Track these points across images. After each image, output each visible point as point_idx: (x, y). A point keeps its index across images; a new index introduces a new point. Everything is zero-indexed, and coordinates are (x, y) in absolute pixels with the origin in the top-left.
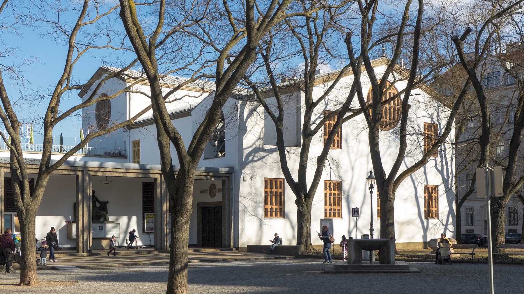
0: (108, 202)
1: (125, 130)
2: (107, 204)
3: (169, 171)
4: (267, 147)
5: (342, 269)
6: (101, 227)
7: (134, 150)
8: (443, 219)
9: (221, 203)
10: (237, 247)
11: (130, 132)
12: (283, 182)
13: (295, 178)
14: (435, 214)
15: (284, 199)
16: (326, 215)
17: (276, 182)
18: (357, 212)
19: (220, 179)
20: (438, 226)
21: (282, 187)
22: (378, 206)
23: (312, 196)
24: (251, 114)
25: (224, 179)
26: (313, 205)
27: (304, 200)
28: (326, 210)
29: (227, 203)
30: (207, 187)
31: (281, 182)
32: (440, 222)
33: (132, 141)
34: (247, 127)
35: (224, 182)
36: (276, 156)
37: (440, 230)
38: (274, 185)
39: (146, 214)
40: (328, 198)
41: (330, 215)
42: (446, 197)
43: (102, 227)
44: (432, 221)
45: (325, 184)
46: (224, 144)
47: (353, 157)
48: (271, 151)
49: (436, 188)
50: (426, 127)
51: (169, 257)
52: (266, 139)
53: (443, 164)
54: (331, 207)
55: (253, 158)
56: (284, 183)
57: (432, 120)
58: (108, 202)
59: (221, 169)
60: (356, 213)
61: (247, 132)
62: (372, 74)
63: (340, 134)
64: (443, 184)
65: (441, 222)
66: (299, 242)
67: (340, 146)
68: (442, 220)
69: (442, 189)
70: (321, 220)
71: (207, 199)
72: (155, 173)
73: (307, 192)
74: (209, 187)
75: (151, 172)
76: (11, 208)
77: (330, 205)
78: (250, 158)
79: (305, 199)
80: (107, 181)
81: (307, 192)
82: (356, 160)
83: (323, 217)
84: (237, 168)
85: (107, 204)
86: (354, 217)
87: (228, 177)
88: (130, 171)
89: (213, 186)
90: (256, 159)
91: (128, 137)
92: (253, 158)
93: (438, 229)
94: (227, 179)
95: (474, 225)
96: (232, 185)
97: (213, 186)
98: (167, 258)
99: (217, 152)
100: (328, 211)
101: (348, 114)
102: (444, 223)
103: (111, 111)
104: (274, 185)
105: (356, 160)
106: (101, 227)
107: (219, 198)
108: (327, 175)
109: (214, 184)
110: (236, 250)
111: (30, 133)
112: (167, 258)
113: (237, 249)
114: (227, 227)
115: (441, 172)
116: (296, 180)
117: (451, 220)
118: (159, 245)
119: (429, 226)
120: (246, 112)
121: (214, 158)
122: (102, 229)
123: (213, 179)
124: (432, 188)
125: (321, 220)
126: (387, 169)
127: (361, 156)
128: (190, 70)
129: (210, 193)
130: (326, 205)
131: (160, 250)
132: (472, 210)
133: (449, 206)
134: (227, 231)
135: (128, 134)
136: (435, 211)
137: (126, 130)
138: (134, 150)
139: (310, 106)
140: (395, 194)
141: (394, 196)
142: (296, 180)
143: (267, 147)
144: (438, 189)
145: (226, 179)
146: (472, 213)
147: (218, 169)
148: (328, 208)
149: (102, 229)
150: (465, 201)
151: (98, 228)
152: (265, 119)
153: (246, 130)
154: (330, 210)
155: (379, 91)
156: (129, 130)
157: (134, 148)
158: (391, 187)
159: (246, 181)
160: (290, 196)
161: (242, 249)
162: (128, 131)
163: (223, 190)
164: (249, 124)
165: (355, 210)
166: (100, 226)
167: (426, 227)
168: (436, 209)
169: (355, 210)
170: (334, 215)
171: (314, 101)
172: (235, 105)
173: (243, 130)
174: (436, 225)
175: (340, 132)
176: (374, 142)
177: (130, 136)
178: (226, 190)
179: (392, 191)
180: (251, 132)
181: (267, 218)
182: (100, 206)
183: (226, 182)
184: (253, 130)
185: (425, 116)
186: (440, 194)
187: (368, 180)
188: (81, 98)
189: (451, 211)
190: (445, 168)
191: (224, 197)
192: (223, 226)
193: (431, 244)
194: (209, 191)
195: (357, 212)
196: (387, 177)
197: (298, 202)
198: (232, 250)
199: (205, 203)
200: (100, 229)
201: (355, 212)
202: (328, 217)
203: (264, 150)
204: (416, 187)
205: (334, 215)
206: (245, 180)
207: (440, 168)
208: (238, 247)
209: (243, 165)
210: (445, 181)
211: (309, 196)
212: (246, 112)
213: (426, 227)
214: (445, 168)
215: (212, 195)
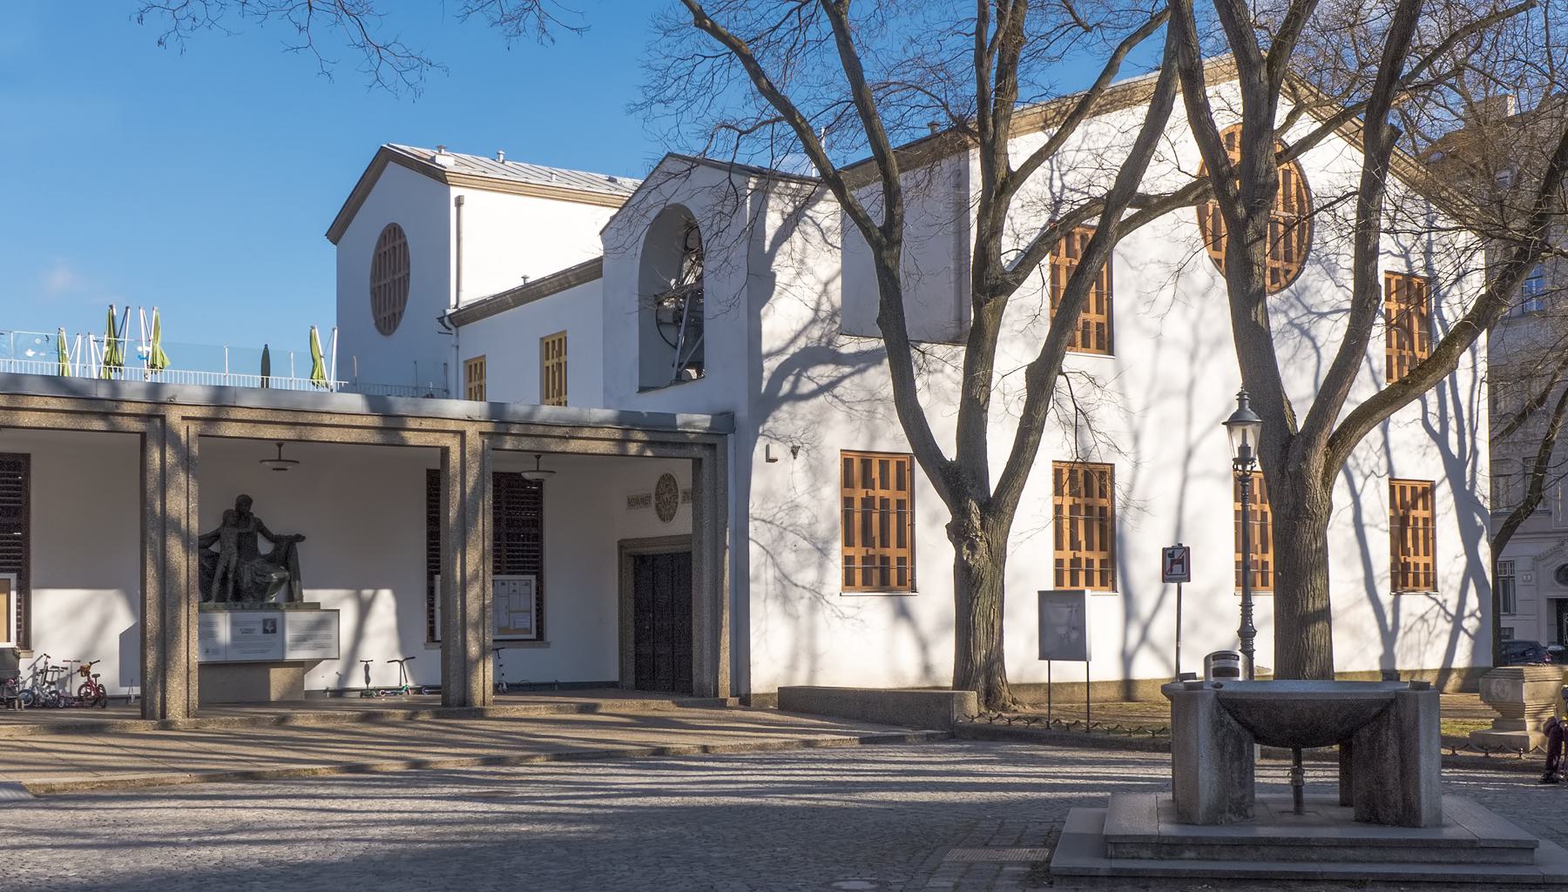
0: (299, 538)
1: (443, 329)
2: (298, 545)
4: (848, 345)
5: (1146, 853)
6: (269, 623)
7: (471, 389)
8: (1446, 597)
9: (686, 539)
10: (743, 692)
11: (457, 335)
12: (907, 467)
13: (949, 450)
14: (1427, 575)
15: (912, 525)
16: (1059, 579)
18: (1180, 562)
19: (682, 452)
20: (1432, 622)
21: (905, 482)
22: (1237, 551)
23: (1007, 510)
24: (791, 223)
25: (697, 452)
26: (1016, 544)
27: (977, 523)
28: (1059, 563)
29: (706, 537)
30: (650, 488)
31: (900, 465)
32: (1438, 607)
33: (466, 362)
34: (774, 275)
35: (698, 463)
36: (880, 378)
37: (1438, 636)
40: (1066, 524)
41: (1074, 582)
42: (1456, 524)
43: (274, 622)
44: (1414, 604)
45: (1058, 474)
46: (703, 341)
47: (1137, 400)
48: (864, 360)
49: (1426, 492)
50: (1393, 288)
52: (846, 319)
53: (1446, 413)
54: (1078, 554)
55: (795, 385)
56: (912, 470)
57: (1409, 264)
58: (299, 538)
59: (681, 419)
60: (1177, 568)
61: (777, 288)
62: (1237, 18)
63: (1105, 302)
64: (1447, 481)
65: (1441, 605)
66: (964, 677)
67: (1105, 343)
68: (1445, 601)
69: (1445, 499)
70: (1043, 596)
72: (441, 428)
73: (992, 494)
74: (655, 486)
75: (412, 424)
76: (8, 558)
77: (1075, 545)
78: (786, 387)
79: (982, 519)
80: (280, 460)
81: (992, 494)
82: (1146, 408)
83: (1049, 585)
84: (743, 414)
85: (298, 545)
86: (1172, 581)
87: (713, 446)
88: (327, 419)
89: (667, 481)
90: (806, 387)
91: (454, 350)
92: (795, 385)
93: (1430, 633)
94: (708, 453)
95: (1514, 615)
96: (726, 473)
97: (667, 481)
99: (680, 365)
100: (1067, 565)
101: (1129, 212)
102: (1452, 610)
103: (408, 274)
104: (876, 473)
105: (1146, 408)
106: (269, 623)
107: (683, 522)
108: (1054, 446)
109: (671, 476)
110: (740, 703)
111: (152, 337)
113: (746, 700)
114: (707, 621)
115: (1440, 439)
116: (950, 452)
117: (1473, 601)
118: (454, 688)
119: (1402, 622)
120: (773, 221)
121: (671, 385)
122: (274, 631)
123: (649, 453)
124: (1414, 489)
125: (1043, 596)
126: (1300, 387)
127: (1165, 395)
129: (657, 506)
130: (1058, 546)
131: (459, 705)
132: (1508, 568)
133: (1467, 553)
134: (707, 635)
135: (453, 340)
136: (1426, 566)
137: (449, 329)
138: (471, 389)
139: (1002, 185)
140: (1331, 488)
141: (1330, 498)
142: (950, 452)
143: (848, 345)
144: (1433, 498)
145: (705, 454)
146: (1509, 577)
147: (674, 416)
148: (1067, 555)
149: (274, 631)
150: (1508, 538)
151: (259, 628)
152: (845, 249)
153: (773, 285)
155: (1266, 83)
156: (457, 327)
157: (470, 381)
158: (1318, 461)
159: (774, 460)
161: (762, 702)
162: (454, 330)
163: (694, 495)
164: (783, 269)
165: (1171, 555)
166: (265, 622)
167: (1390, 628)
168: (1428, 560)
169: (1171, 555)
170: (1089, 583)
171: (1015, 167)
172: (727, 182)
173: (761, 285)
174: (1427, 621)
175: (1105, 297)
176: (1249, 285)
177: (458, 347)
178: (707, 493)
179: (1323, 480)
180: (792, 290)
181: (850, 591)
182: (276, 549)
183: (705, 463)
184: (798, 282)
185: (1389, 252)
186: (1439, 509)
187: (1230, 430)
188: (335, 243)
189: (1473, 567)
190: (1453, 424)
192: (695, 620)
193: (1494, 691)
194: (657, 499)
195: (1180, 562)
196: (1300, 425)
197: (959, 533)
198: (722, 704)
199: (642, 541)
200: (266, 631)
201: (1173, 562)
202: (1067, 586)
203: (837, 359)
204: (1358, 491)
205: (1089, 583)
206: (771, 456)
207: (1437, 428)
208: (748, 695)
209: (767, 404)
210: (1456, 468)
211: (999, 508)
212: (773, 221)
213: (1390, 628)
214: (1453, 424)
215: (666, 515)
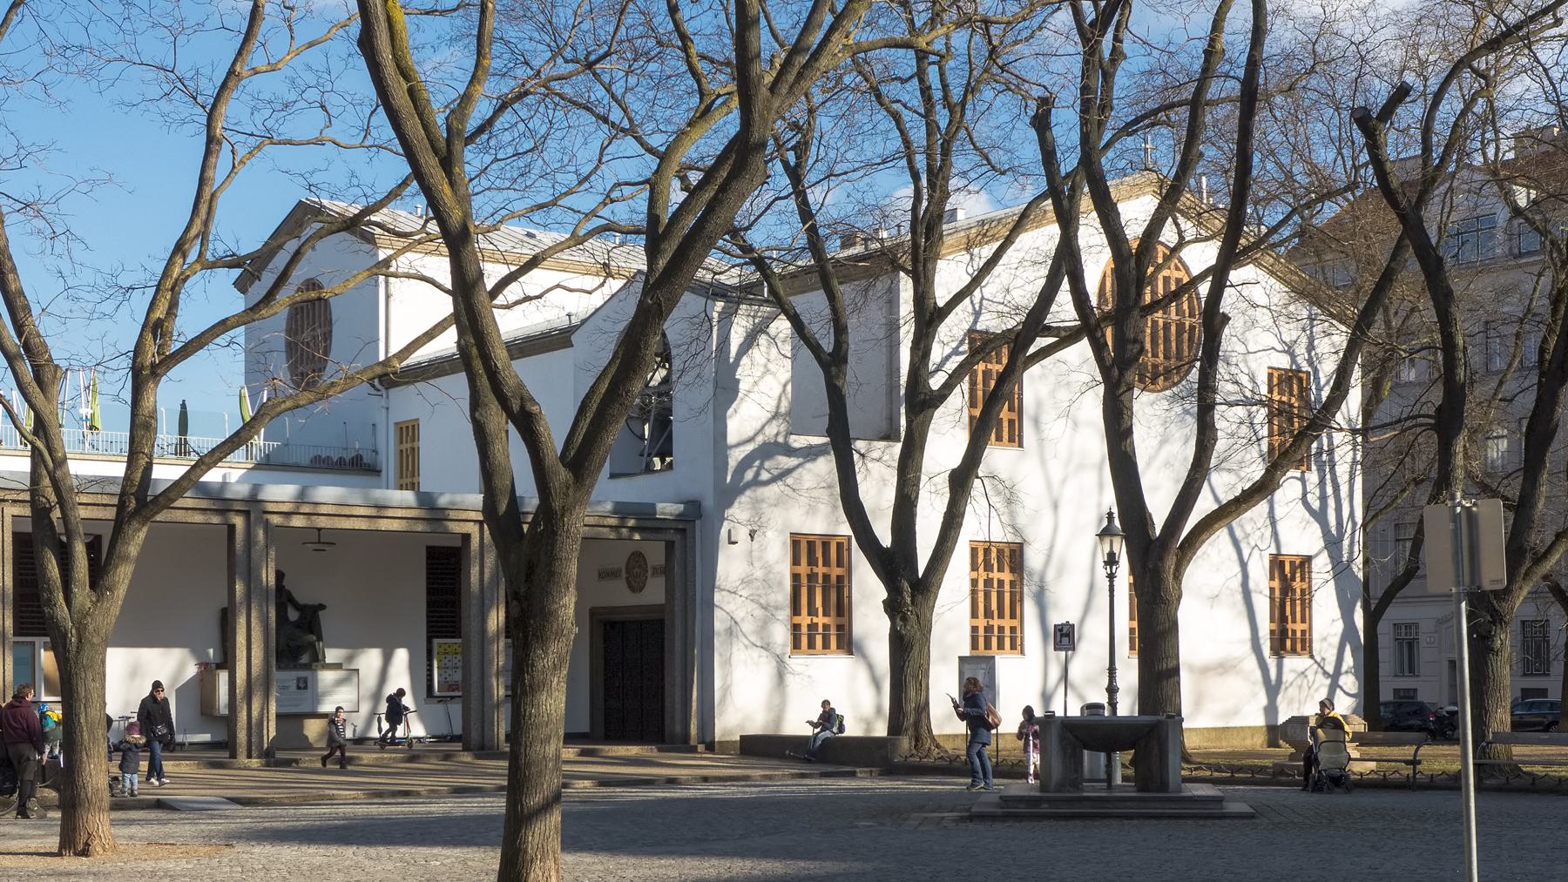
0: (322, 607)
1: (373, 391)
2: (320, 613)
3: (505, 512)
4: (798, 441)
5: (1023, 806)
6: (301, 682)
7: (402, 451)
8: (1324, 656)
9: (660, 608)
10: (708, 740)
11: (388, 397)
12: (846, 547)
13: (884, 534)
14: (1303, 641)
15: (850, 597)
16: (974, 646)
17: (826, 545)
18: (1067, 635)
19: (659, 536)
20: (1311, 678)
21: (843, 560)
22: (1131, 619)
23: (933, 589)
24: (750, 341)
25: (671, 536)
26: (938, 614)
27: (909, 600)
28: (974, 629)
29: (678, 609)
30: (620, 562)
31: (839, 545)
32: (1316, 666)
33: (396, 424)
34: (738, 381)
35: (670, 546)
36: (826, 467)
37: (1317, 690)
38: (819, 554)
39: (436, 641)
40: (981, 595)
41: (988, 646)
42: (1334, 592)
43: (305, 680)
44: (1293, 663)
45: (974, 551)
46: (671, 431)
47: (1056, 471)
48: (811, 453)
49: (1304, 564)
50: (1275, 381)
51: (506, 772)
52: (795, 418)
53: (1326, 492)
54: (991, 622)
55: (757, 474)
56: (849, 550)
57: (1293, 360)
58: (322, 607)
59: (660, 506)
60: (1065, 640)
61: (740, 395)
62: (1112, 223)
63: (1016, 401)
64: (1325, 553)
65: (1319, 665)
66: (895, 726)
67: (1016, 439)
68: (1323, 659)
69: (1322, 566)
70: (962, 659)
71: (619, 596)
72: (464, 518)
73: (920, 576)
74: (626, 560)
75: (453, 515)
76: (33, 623)
77: (988, 614)
78: (749, 475)
79: (913, 597)
80: (319, 542)
81: (920, 576)
82: (1064, 481)
83: (966, 652)
84: (709, 503)
85: (320, 613)
86: (1061, 650)
87: (683, 531)
88: (390, 513)
89: (637, 558)
90: (765, 476)
91: (384, 411)
92: (757, 474)
93: (1310, 688)
94: (679, 537)
95: (1418, 676)
96: (695, 556)
97: (637, 558)
98: (501, 775)
99: (649, 455)
100: (981, 632)
101: (1041, 342)
102: (1330, 669)
103: (331, 332)
104: (819, 554)
105: (1064, 481)
106: (301, 682)
107: (654, 593)
108: (977, 525)
109: (641, 553)
110: (706, 749)
111: (90, 398)
112: (501, 775)
113: (711, 746)
114: (678, 680)
115: (1320, 516)
116: (886, 539)
117: (1348, 661)
118: (475, 735)
119: (1284, 679)
120: (737, 337)
121: (640, 474)
122: (306, 688)
123: (637, 537)
124: (1292, 563)
125: (962, 659)
126: (1159, 506)
127: (1081, 467)
128: (569, 209)
129: (627, 578)
130: (974, 615)
131: (478, 750)
132: (1413, 630)
133: (1343, 617)
134: (678, 692)
135: (383, 402)
136: (1303, 632)
137: (378, 390)
138: (402, 451)
139: (929, 317)
140: (1181, 581)
141: (1180, 588)
142: (886, 539)
143: (798, 441)
144: (1310, 567)
145: (677, 538)
146: (1414, 639)
147: (653, 506)
148: (981, 623)
149: (306, 688)
150: (1390, 602)
151: (293, 685)
152: (794, 358)
153: (736, 391)
154: (989, 629)
155: (1134, 272)
156: (386, 389)
157: (402, 443)
158: (1171, 562)
159: (735, 543)
160: (868, 589)
161: (725, 746)
162: (384, 392)
163: (666, 570)
164: (746, 373)
165: (1061, 630)
166: (298, 679)
167: (1273, 682)
168: (1305, 626)
169: (1061, 630)
170: (1001, 646)
171: (941, 303)
172: (703, 315)
173: (726, 390)
174: (1306, 676)
175: (1016, 396)
176: (1120, 425)
177: (388, 409)
178: (677, 570)
179: (1174, 574)
180: (751, 395)
181: (798, 654)
182: (301, 617)
183: (677, 546)
184: (756, 389)
185: (1273, 348)
186: (1316, 583)
187: (1101, 540)
188: (243, 293)
189: (1349, 632)
190: (1331, 503)
191: (670, 591)
192: (667, 679)
193: (1289, 733)
194: (627, 572)
195: (1067, 635)
196: (1158, 532)
197: (893, 607)
198: (694, 750)
199: (613, 610)
200: (299, 688)
201: (1062, 636)
202: (981, 651)
203: (789, 451)
204: (1246, 560)
205: (1001, 646)
206: (733, 539)
207: (1316, 505)
208: (713, 742)
209: (728, 495)
210: (1332, 543)
211: (925, 587)
212: (737, 337)
213: (1273, 682)
214: (1331, 503)
215: (636, 585)
